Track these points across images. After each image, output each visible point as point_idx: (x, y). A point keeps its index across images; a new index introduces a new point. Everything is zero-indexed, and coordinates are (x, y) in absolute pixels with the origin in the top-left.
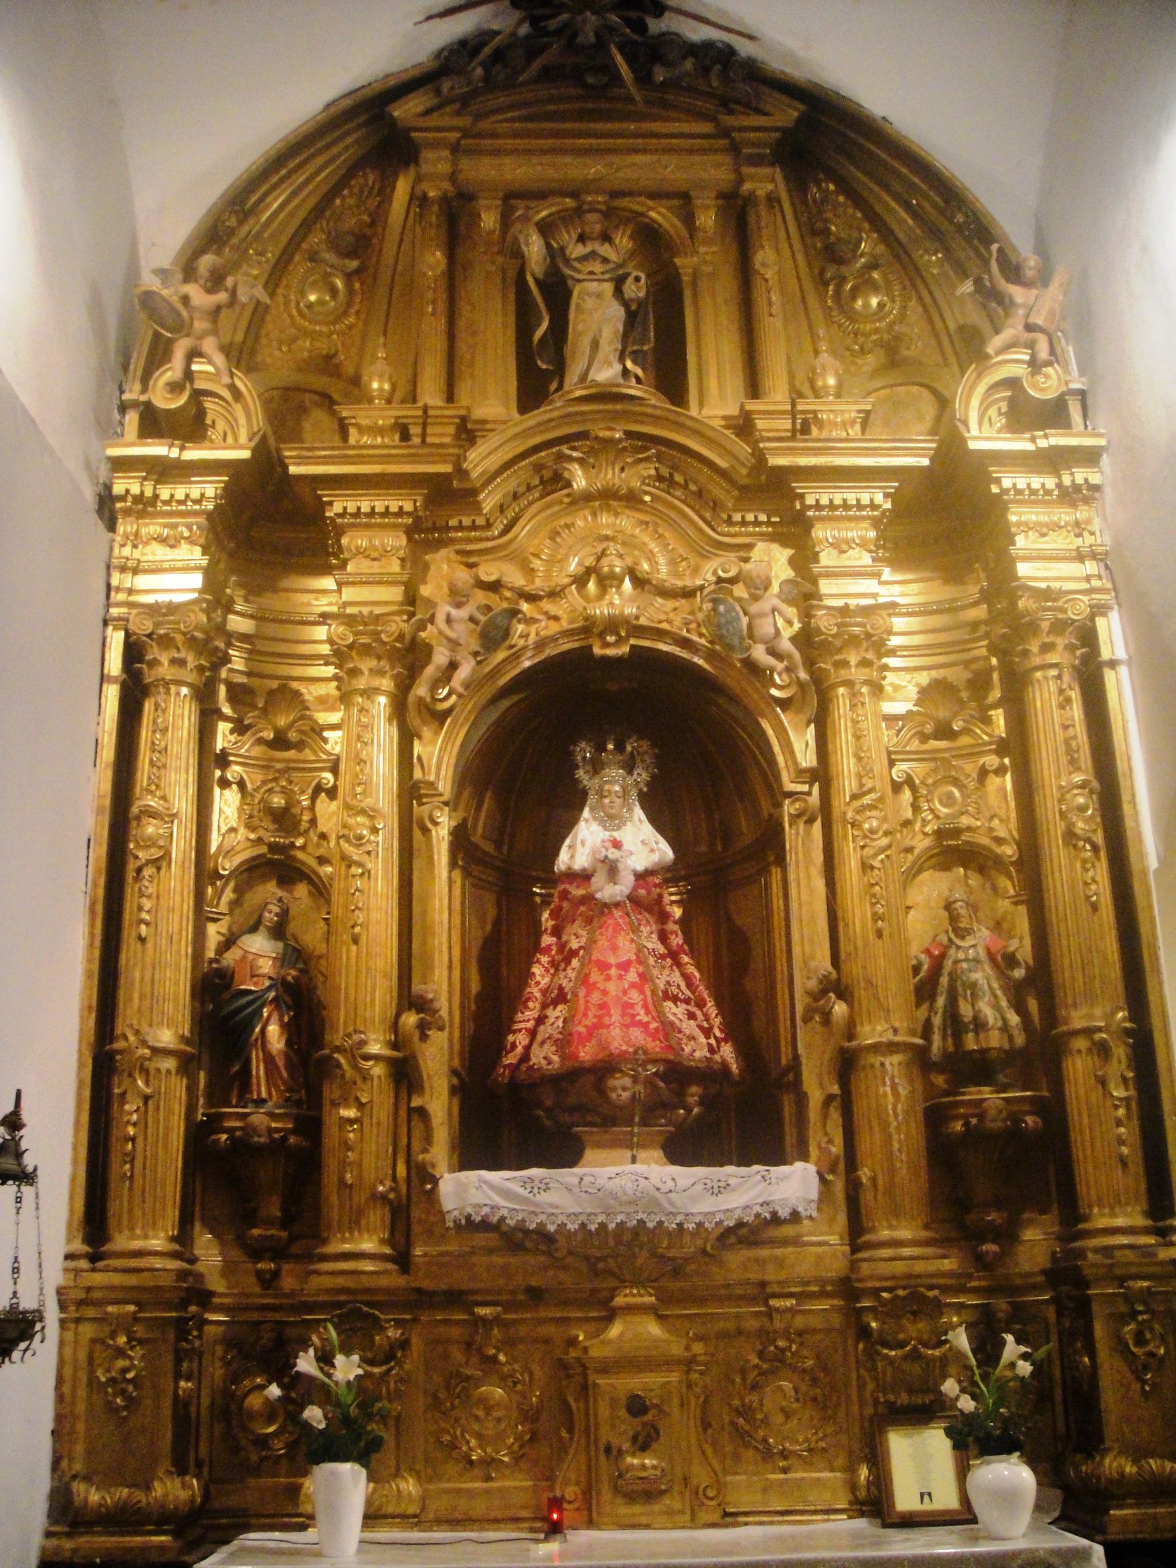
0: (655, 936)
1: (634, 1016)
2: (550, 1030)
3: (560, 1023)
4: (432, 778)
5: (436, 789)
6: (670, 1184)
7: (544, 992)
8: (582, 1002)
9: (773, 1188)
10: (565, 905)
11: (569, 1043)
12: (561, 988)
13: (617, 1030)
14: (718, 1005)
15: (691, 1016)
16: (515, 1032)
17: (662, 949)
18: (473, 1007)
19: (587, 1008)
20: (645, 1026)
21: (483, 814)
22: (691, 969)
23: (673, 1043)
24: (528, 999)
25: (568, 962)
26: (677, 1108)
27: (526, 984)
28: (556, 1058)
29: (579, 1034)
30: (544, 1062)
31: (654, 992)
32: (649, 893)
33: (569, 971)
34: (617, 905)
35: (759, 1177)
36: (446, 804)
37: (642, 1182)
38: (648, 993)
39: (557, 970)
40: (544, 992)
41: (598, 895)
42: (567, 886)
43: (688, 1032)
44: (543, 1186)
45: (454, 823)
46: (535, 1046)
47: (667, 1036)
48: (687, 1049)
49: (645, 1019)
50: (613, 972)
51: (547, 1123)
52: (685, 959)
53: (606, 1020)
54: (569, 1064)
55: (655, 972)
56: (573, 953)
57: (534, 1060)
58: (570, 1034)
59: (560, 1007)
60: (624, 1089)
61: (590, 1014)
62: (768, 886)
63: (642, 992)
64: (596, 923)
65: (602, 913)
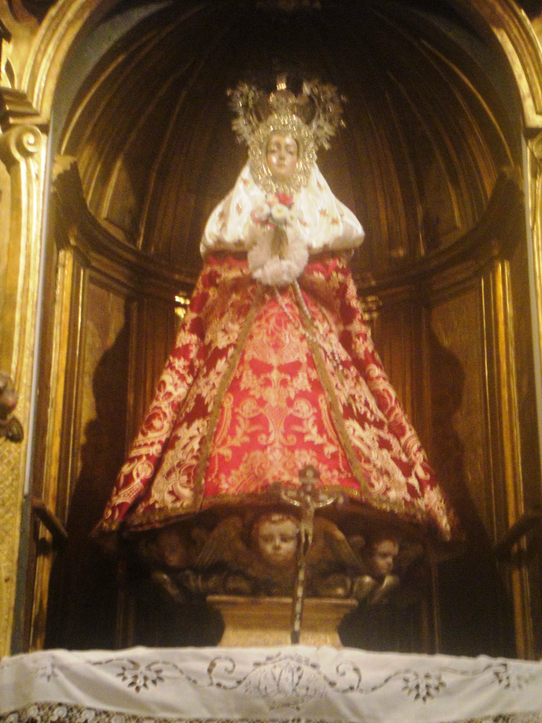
0: (334, 338)
1: (300, 436)
2: (181, 456)
3: (196, 446)
4: (24, 87)
5: (30, 105)
6: (352, 677)
7: (177, 407)
8: (228, 414)
9: (512, 693)
10: (212, 293)
11: (208, 471)
12: (200, 399)
13: (277, 454)
14: (420, 434)
15: (384, 444)
16: (132, 460)
17: (344, 355)
18: (83, 439)
19: (234, 422)
20: (319, 449)
21: (110, 191)
22: (383, 385)
23: (358, 473)
24: (154, 416)
25: (211, 364)
26: (361, 574)
27: (153, 396)
28: (186, 493)
29: (222, 458)
30: (169, 499)
31: (331, 407)
32: (328, 279)
33: (212, 375)
34: (284, 289)
35: (489, 675)
36: (44, 128)
37: (307, 670)
38: (324, 407)
39: (196, 378)
40: (177, 407)
41: (258, 274)
42: (217, 268)
43: (379, 464)
44: (152, 675)
45: (58, 169)
46: (159, 478)
47: (348, 467)
48: (379, 486)
49: (319, 440)
50: (275, 376)
51: (173, 591)
52: (376, 371)
53: (262, 439)
54: (205, 502)
55: (335, 381)
56: (221, 353)
57: (155, 496)
58: (210, 459)
59: (197, 423)
60: (284, 539)
61: (239, 431)
62: (490, 289)
63: (315, 404)
64: (253, 313)
65: (263, 301)
